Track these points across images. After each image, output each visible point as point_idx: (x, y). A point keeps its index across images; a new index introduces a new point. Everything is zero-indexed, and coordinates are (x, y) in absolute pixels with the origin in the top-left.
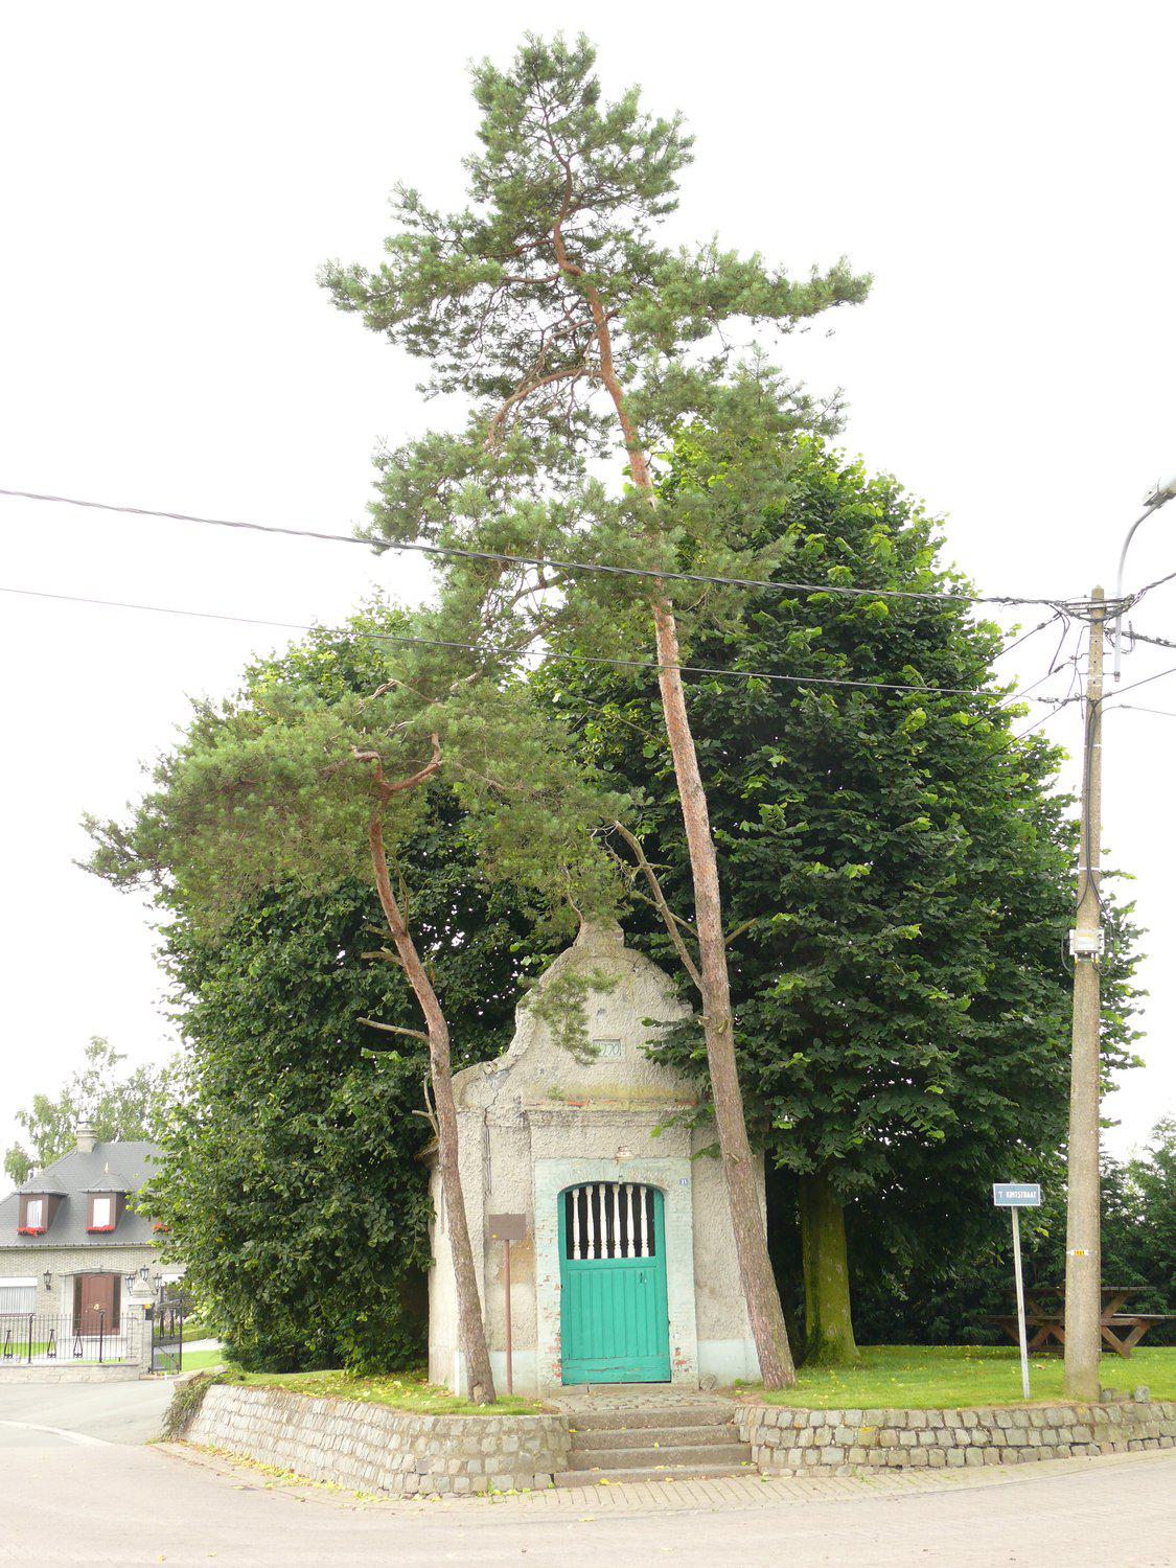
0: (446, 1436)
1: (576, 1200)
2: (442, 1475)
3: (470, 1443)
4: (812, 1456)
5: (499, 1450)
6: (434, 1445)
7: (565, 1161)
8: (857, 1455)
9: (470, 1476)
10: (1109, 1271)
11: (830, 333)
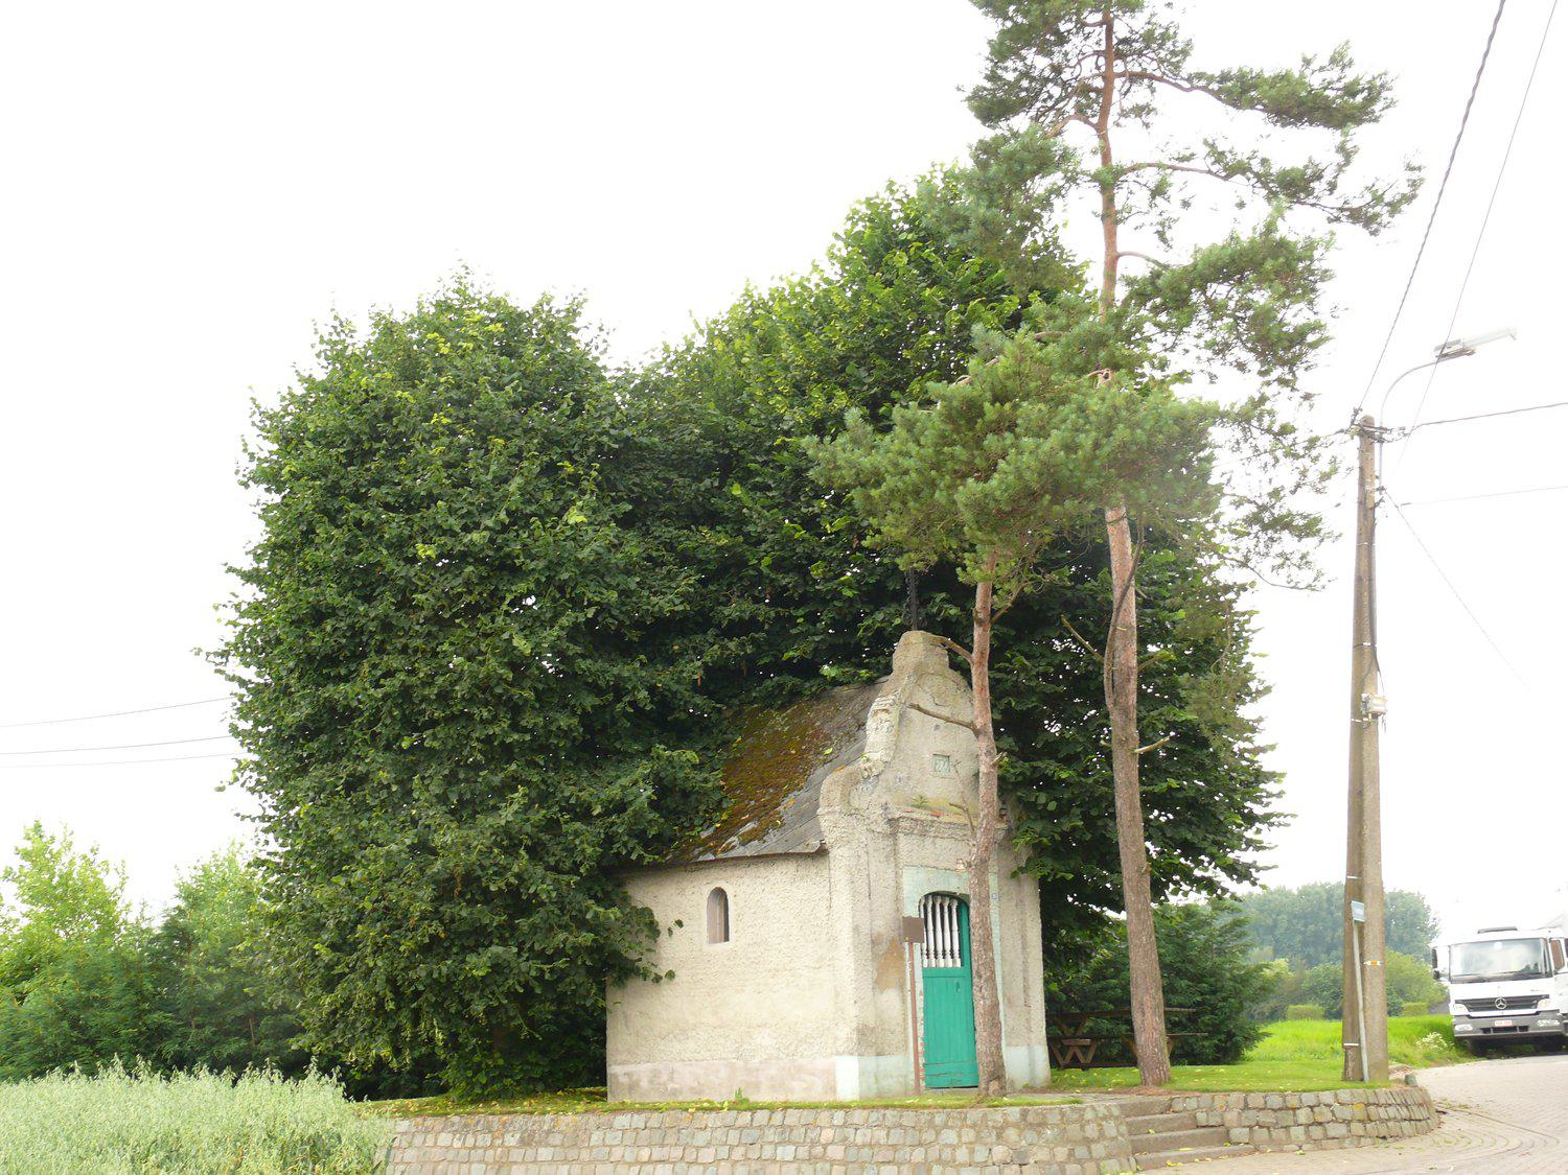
0: (1043, 1124)
2: (1049, 1163)
3: (1074, 1130)
4: (1317, 1132)
5: (1102, 1135)
6: (1031, 1135)
8: (1357, 1128)
9: (1079, 1161)
10: (1122, 1010)
11: (1169, 5)
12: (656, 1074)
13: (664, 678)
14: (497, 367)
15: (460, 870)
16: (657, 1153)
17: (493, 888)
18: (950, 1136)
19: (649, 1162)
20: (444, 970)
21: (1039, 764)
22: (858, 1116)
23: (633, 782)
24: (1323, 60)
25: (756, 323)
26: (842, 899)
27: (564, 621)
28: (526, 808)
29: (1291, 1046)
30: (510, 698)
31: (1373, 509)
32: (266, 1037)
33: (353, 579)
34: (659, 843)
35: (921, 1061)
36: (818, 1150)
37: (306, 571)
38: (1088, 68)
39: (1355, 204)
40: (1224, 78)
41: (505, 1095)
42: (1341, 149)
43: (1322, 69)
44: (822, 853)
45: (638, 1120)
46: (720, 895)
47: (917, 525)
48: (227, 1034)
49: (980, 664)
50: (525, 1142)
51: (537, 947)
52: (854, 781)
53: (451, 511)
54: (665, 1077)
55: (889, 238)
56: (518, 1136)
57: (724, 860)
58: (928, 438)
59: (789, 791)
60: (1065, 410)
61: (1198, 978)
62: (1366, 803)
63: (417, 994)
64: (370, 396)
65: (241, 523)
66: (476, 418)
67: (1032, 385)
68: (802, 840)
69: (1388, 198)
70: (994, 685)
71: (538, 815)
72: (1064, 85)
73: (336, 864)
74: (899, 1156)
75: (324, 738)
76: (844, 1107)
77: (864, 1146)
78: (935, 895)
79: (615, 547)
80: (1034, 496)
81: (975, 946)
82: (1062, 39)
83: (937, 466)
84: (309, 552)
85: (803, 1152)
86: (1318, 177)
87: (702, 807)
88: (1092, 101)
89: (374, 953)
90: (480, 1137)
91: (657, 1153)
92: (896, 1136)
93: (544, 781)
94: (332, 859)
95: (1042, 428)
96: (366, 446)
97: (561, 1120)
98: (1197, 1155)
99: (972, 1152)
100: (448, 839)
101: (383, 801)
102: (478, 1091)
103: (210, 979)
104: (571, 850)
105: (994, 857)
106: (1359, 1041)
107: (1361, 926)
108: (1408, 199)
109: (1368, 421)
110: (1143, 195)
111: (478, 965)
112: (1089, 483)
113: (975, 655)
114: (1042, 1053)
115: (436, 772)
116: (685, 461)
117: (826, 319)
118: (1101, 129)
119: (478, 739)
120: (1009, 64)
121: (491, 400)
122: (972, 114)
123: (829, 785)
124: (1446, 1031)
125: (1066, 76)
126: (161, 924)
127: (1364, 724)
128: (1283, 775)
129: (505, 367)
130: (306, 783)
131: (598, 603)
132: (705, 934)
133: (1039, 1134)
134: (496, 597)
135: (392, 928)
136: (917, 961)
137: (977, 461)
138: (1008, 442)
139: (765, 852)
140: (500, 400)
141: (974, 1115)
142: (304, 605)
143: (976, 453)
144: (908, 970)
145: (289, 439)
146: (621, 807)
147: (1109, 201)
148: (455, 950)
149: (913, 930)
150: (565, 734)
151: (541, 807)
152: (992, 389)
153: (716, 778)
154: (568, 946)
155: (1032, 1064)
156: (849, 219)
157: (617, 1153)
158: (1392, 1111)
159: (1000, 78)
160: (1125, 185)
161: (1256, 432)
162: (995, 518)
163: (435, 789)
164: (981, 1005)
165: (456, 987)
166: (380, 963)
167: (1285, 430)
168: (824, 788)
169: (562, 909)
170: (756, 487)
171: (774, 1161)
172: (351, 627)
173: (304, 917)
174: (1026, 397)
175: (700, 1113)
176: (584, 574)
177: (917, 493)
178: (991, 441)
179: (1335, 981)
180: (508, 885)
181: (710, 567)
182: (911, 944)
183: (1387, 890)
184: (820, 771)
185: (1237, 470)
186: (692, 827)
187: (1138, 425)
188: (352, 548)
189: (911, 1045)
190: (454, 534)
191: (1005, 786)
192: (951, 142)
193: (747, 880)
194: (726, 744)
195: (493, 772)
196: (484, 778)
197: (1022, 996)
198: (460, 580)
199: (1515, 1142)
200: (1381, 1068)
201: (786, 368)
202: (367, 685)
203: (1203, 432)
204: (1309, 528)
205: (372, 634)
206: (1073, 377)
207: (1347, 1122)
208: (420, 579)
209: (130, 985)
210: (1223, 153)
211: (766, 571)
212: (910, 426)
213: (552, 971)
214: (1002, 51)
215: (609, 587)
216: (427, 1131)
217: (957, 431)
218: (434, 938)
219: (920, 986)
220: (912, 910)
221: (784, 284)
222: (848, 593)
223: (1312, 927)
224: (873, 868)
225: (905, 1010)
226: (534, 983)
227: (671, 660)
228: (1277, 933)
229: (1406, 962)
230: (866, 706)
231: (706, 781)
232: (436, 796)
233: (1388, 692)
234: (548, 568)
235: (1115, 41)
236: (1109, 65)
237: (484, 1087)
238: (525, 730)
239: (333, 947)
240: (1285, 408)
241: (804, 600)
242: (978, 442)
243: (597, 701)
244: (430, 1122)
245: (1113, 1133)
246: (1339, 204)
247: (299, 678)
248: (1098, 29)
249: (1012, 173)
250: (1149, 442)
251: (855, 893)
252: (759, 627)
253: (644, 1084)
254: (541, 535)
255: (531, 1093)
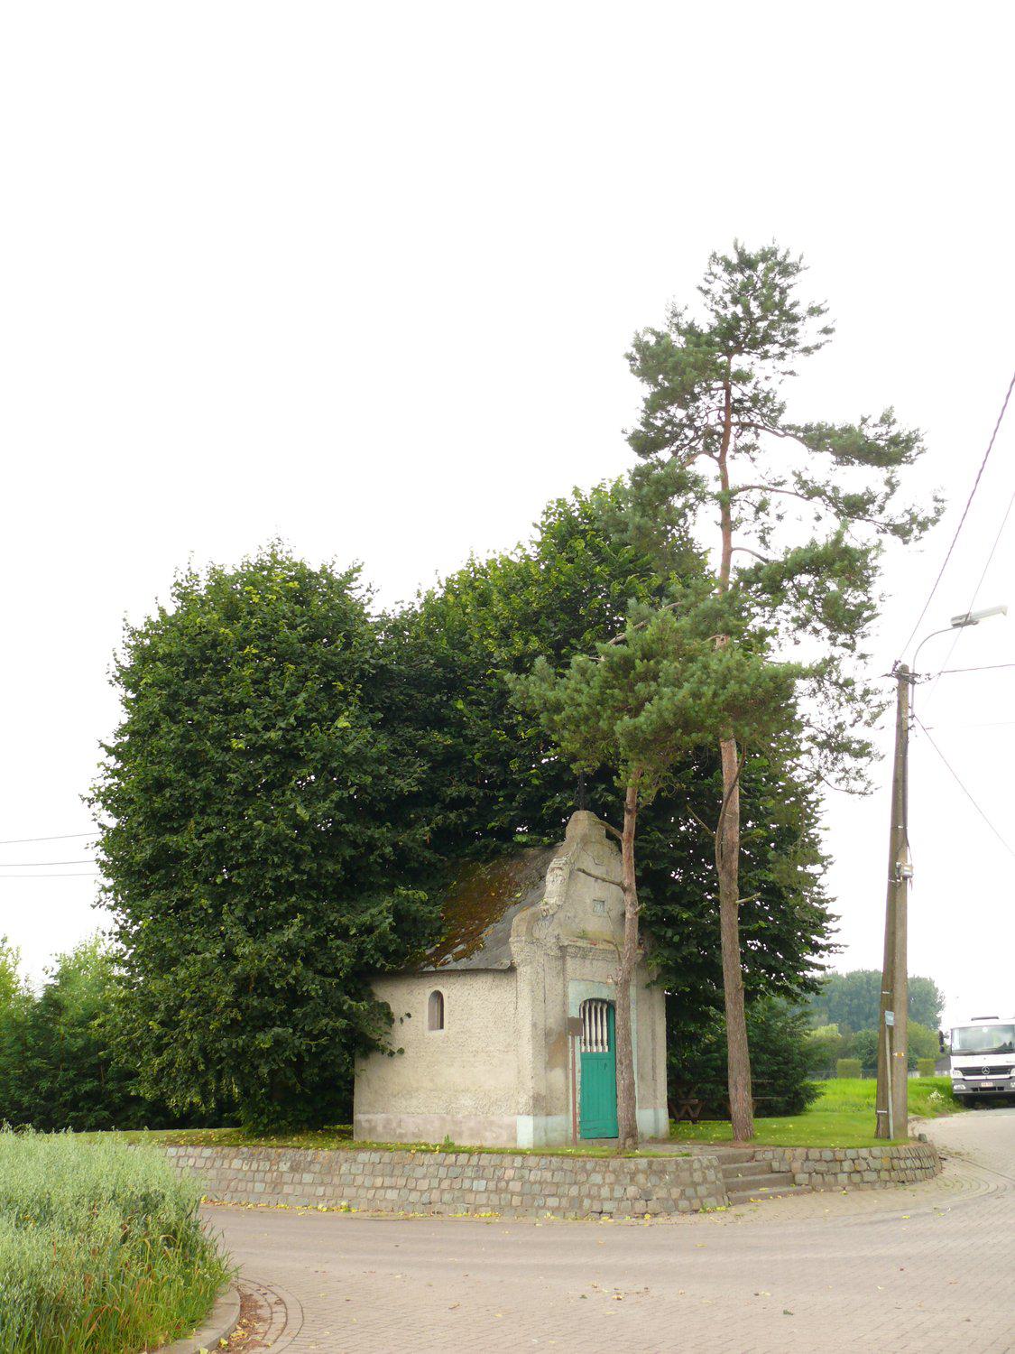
0: (663, 1172)
2: (667, 1199)
3: (685, 1175)
4: (856, 1178)
5: (705, 1180)
6: (654, 1179)
8: (884, 1175)
9: (689, 1199)
12: (388, 1122)
13: (403, 838)
14: (293, 612)
15: (254, 972)
16: (388, 1181)
17: (277, 986)
18: (597, 1178)
19: (382, 1187)
20: (241, 1042)
21: (668, 907)
22: (532, 1161)
23: (378, 912)
24: (876, 419)
25: (477, 584)
26: (525, 1004)
27: (334, 796)
28: (302, 929)
29: (841, 1097)
30: (294, 850)
31: (907, 731)
32: (113, 1080)
33: (185, 761)
34: (397, 956)
35: (578, 1120)
36: (503, 1184)
37: (152, 754)
38: (713, 419)
39: (898, 521)
40: (808, 429)
41: (282, 1133)
42: (889, 482)
43: (875, 426)
44: (511, 970)
45: (375, 1157)
46: (438, 996)
47: (586, 741)
48: (85, 1076)
49: (628, 841)
50: (293, 1169)
51: (306, 1028)
52: (536, 919)
53: (255, 715)
54: (395, 1124)
55: (572, 528)
56: (288, 1164)
57: (442, 972)
58: (596, 682)
59: (489, 923)
60: (693, 667)
61: (775, 1053)
62: (897, 941)
63: (221, 1060)
64: (203, 631)
65: (109, 713)
66: (275, 648)
67: (671, 648)
68: (497, 959)
69: (920, 518)
70: (637, 850)
71: (311, 935)
72: (697, 430)
73: (166, 964)
74: (560, 1191)
75: (163, 872)
76: (521, 1153)
77: (535, 1183)
78: (591, 1001)
79: (372, 743)
80: (670, 730)
81: (618, 1042)
82: (695, 398)
83: (601, 702)
84: (154, 741)
85: (492, 1185)
86: (872, 501)
87: (428, 931)
88: (715, 441)
89: (191, 1029)
90: (262, 1163)
91: (388, 1181)
92: (558, 1177)
93: (316, 909)
94: (164, 960)
95: (677, 679)
96: (198, 666)
97: (320, 1154)
98: (771, 1194)
99: (612, 1190)
100: (246, 950)
101: (201, 919)
102: (261, 1128)
103: (73, 1036)
104: (333, 960)
105: (634, 974)
106: (888, 1109)
107: (891, 1028)
108: (934, 522)
109: (904, 668)
110: (749, 512)
111: (264, 1040)
112: (709, 722)
113: (625, 835)
114: (663, 1113)
115: (240, 902)
116: (420, 681)
117: (526, 585)
118: (721, 461)
119: (270, 879)
120: (658, 415)
121: (287, 637)
122: (631, 448)
123: (518, 921)
124: (945, 1089)
125: (697, 424)
126: (41, 996)
127: (897, 884)
128: (838, 917)
129: (298, 613)
130: (148, 904)
131: (357, 784)
132: (426, 1023)
133: (661, 1178)
134: (286, 778)
135: (205, 1012)
136: (578, 1048)
137: (630, 700)
138: (652, 689)
139: (471, 967)
140: (293, 637)
141: (615, 1163)
142: (149, 777)
143: (630, 694)
144: (571, 1055)
145: (145, 657)
146: (369, 930)
147: (726, 514)
148: (249, 1029)
149: (575, 1027)
150: (333, 875)
151: (313, 927)
152: (642, 650)
153: (438, 911)
154: (329, 1028)
155: (656, 1121)
156: (544, 513)
157: (359, 1180)
158: (909, 1163)
159: (653, 424)
160: (738, 503)
161: (827, 683)
162: (640, 744)
163: (238, 913)
164: (621, 1084)
165: (249, 1056)
166: (195, 1037)
167: (849, 683)
168: (515, 921)
169: (326, 1002)
170: (472, 703)
171: (471, 1190)
172: (183, 794)
173: (142, 1001)
174: (666, 656)
175: (419, 1154)
176: (348, 763)
177: (587, 719)
178: (640, 687)
179: (871, 1042)
180: (288, 984)
181: (439, 758)
182: (573, 1036)
183: (909, 976)
184: (512, 910)
185: (811, 707)
186: (420, 946)
187: (744, 681)
188: (185, 738)
189: (571, 1108)
190: (257, 732)
191: (643, 924)
192: (619, 464)
193: (458, 986)
194: (445, 886)
195: (280, 902)
196: (274, 906)
197: (651, 1058)
198: (261, 764)
199: (993, 1187)
200: (902, 1128)
201: (496, 618)
202: (193, 836)
203: (792, 686)
204: (863, 751)
205: (197, 801)
206: (699, 640)
207: (878, 1171)
208: (233, 763)
209: (18, 1039)
210: (806, 482)
211: (477, 763)
212: (583, 672)
213: (317, 1046)
214: (653, 405)
215: (365, 773)
216: (224, 1158)
217: (616, 678)
218: (234, 1021)
219: (578, 1066)
220: (574, 1012)
221: (496, 556)
222: (536, 782)
223: (856, 1001)
224: (547, 981)
225: (567, 1078)
226: (305, 1054)
227: (409, 825)
228: (831, 1005)
229: (920, 1029)
230: (546, 863)
231: (431, 912)
232: (238, 918)
233: (917, 858)
234: (322, 758)
235: (732, 401)
236: (728, 417)
237: (265, 1126)
238: (303, 872)
239: (162, 1023)
240: (848, 667)
241: (503, 785)
242: (631, 688)
243: (353, 852)
244: (226, 1151)
245: (713, 1178)
246: (887, 521)
247: (145, 829)
248: (720, 392)
249: (658, 491)
250: (752, 693)
251: (534, 999)
252: (472, 803)
253: (380, 1129)
254: (318, 735)
255: (298, 1131)
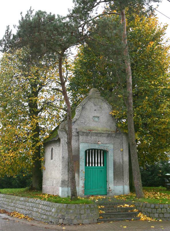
1: (93, 153)
7: (86, 144)
